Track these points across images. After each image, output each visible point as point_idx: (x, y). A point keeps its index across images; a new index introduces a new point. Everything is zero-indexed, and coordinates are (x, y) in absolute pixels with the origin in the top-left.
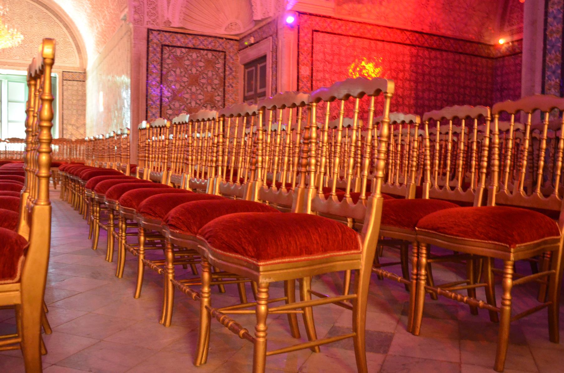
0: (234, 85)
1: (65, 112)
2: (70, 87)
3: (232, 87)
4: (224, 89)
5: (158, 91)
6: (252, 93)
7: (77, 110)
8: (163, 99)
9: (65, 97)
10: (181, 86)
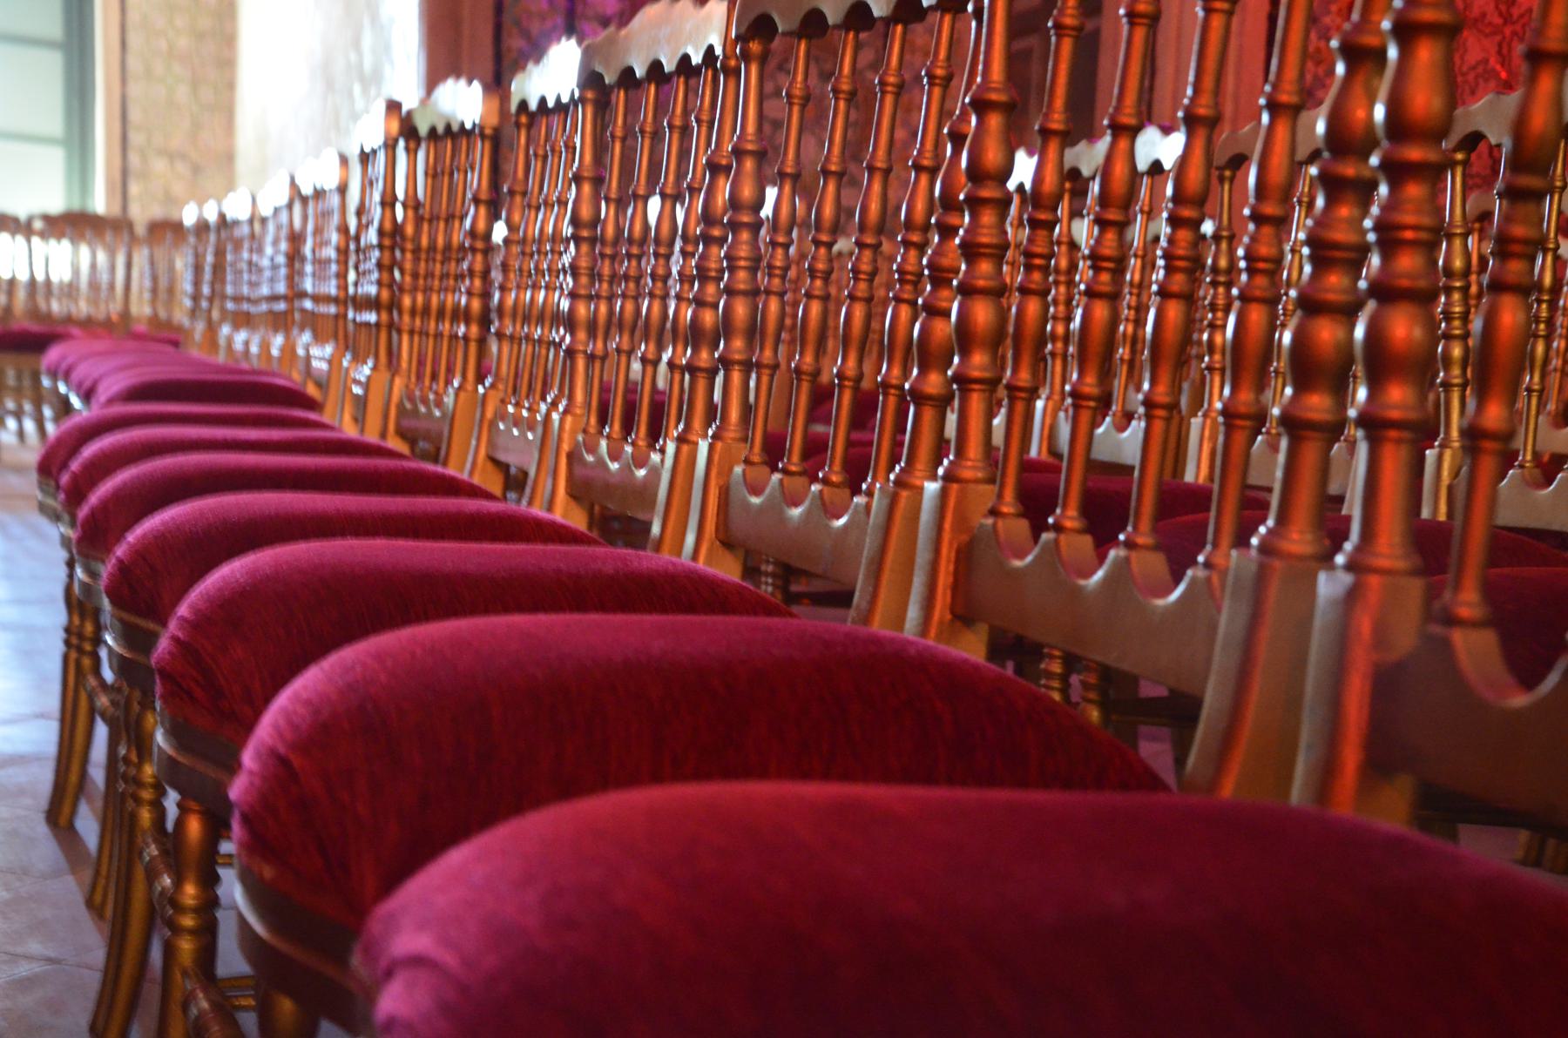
1: (135, 90)
7: (195, 84)
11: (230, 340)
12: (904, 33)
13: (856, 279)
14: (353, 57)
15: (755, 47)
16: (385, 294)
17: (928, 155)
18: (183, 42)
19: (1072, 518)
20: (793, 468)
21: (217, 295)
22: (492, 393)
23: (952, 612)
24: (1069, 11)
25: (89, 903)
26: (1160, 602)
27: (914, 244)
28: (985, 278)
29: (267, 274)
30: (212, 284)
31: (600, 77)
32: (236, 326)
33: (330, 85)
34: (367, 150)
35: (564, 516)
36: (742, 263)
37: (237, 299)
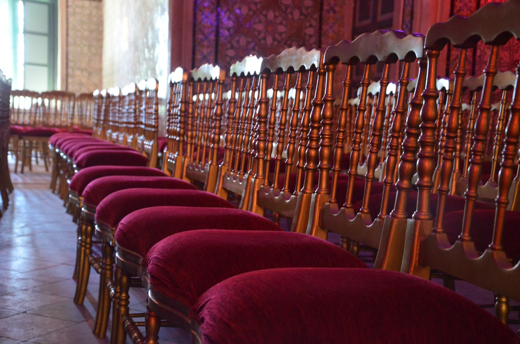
0: (337, 9)
1: (71, 48)
2: (78, 10)
3: (334, 12)
4: (321, 16)
5: (213, 17)
6: (366, 22)
7: (90, 47)
8: (221, 31)
9: (71, 25)
10: (250, 10)
11: (111, 135)
12: (389, 66)
13: (373, 146)
14: (145, 40)
15: (331, 67)
16: (182, 131)
17: (400, 108)
18: (86, 33)
19: (467, 236)
20: (348, 206)
21: (106, 120)
22: (223, 167)
23: (419, 262)
24: (461, 69)
25: (94, 332)
26: (509, 270)
27: (396, 137)
28: (429, 153)
29: (126, 115)
30: (105, 115)
31: (269, 70)
32: (114, 131)
33: (136, 49)
34: (173, 82)
35: (256, 212)
36: (327, 136)
37: (114, 122)
